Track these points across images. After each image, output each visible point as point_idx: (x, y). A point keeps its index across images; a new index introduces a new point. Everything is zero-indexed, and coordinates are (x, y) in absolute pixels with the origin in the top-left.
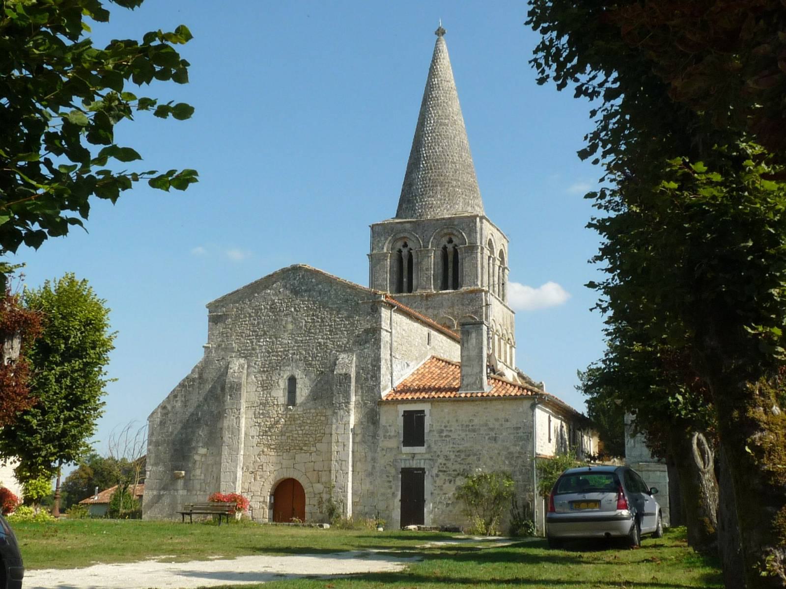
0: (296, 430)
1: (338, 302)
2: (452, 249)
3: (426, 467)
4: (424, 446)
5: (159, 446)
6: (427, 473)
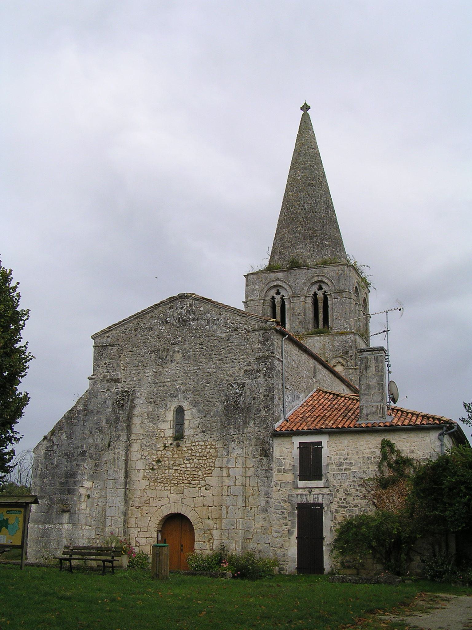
0: (185, 463)
1: (228, 331)
2: (322, 296)
3: (325, 502)
4: (322, 480)
5: (44, 478)
6: (326, 508)
